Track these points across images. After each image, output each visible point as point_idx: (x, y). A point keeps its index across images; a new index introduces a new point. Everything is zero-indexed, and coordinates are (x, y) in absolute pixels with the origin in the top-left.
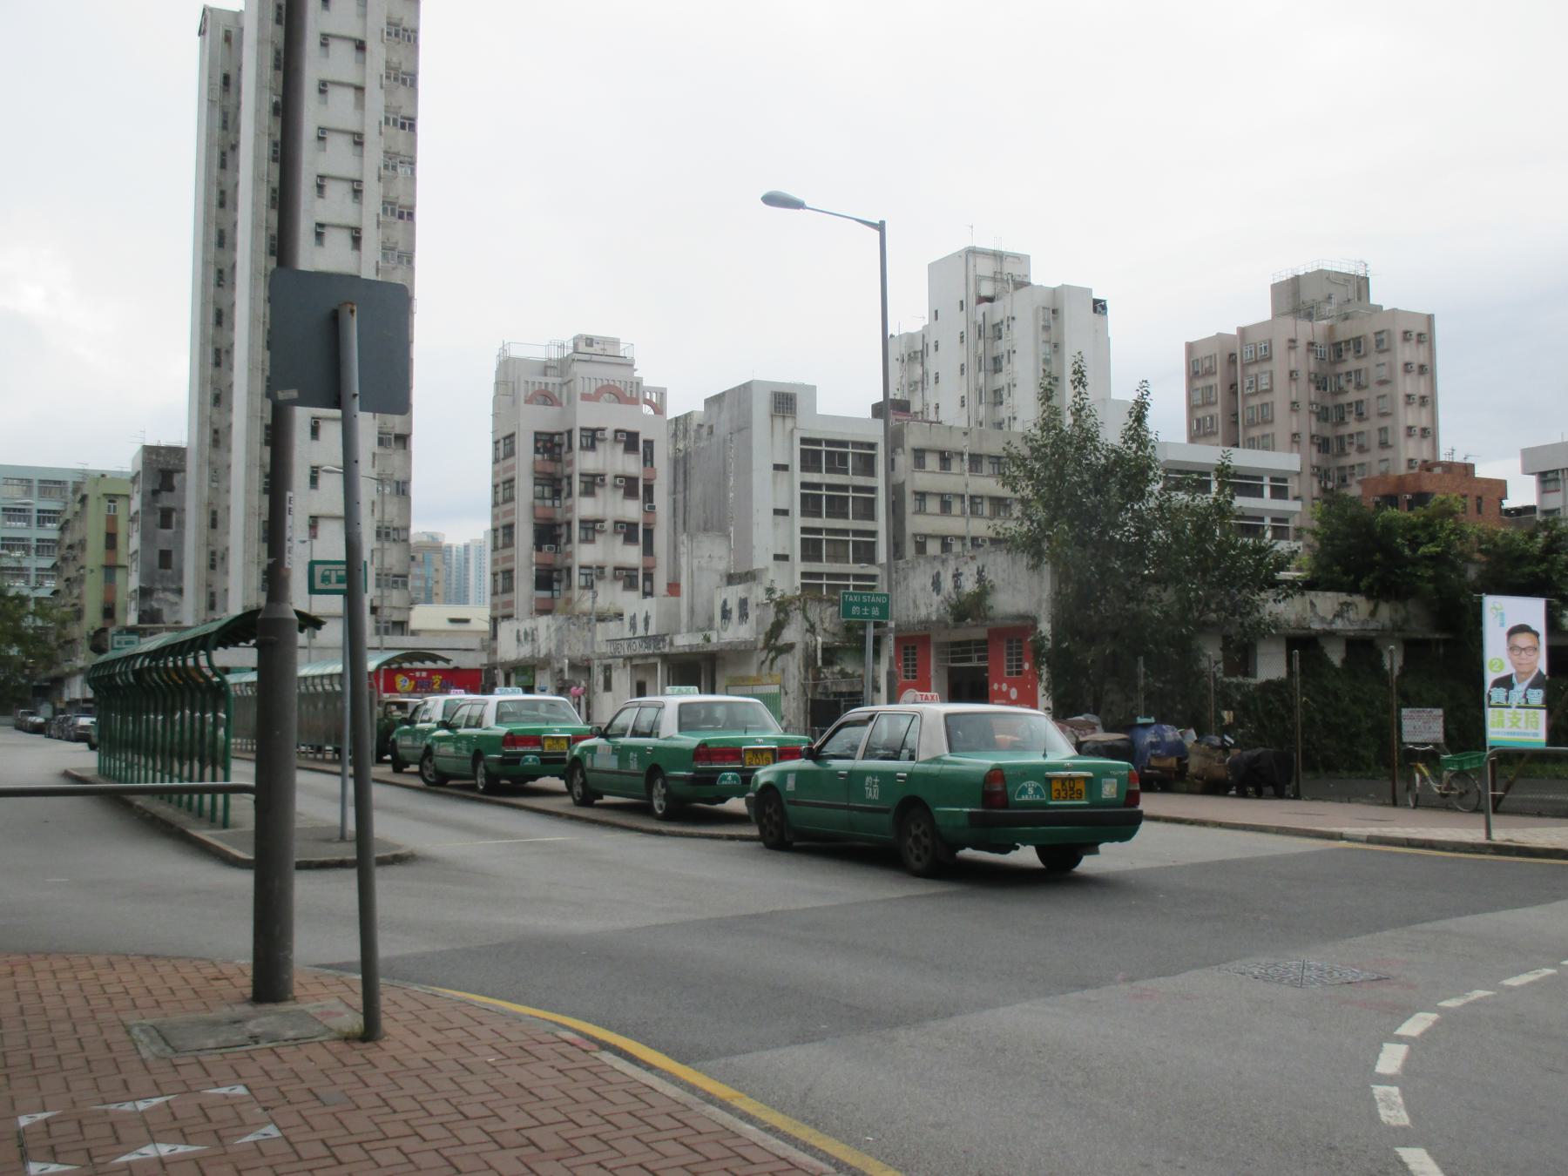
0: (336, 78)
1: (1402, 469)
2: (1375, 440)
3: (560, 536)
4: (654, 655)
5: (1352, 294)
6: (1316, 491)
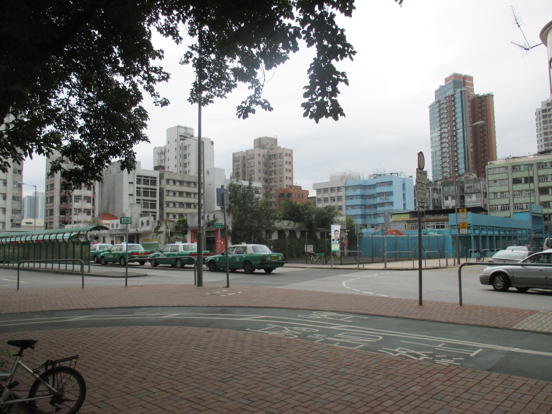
1: (285, 187)
2: (278, 180)
3: (68, 200)
4: (123, 234)
6: (264, 192)
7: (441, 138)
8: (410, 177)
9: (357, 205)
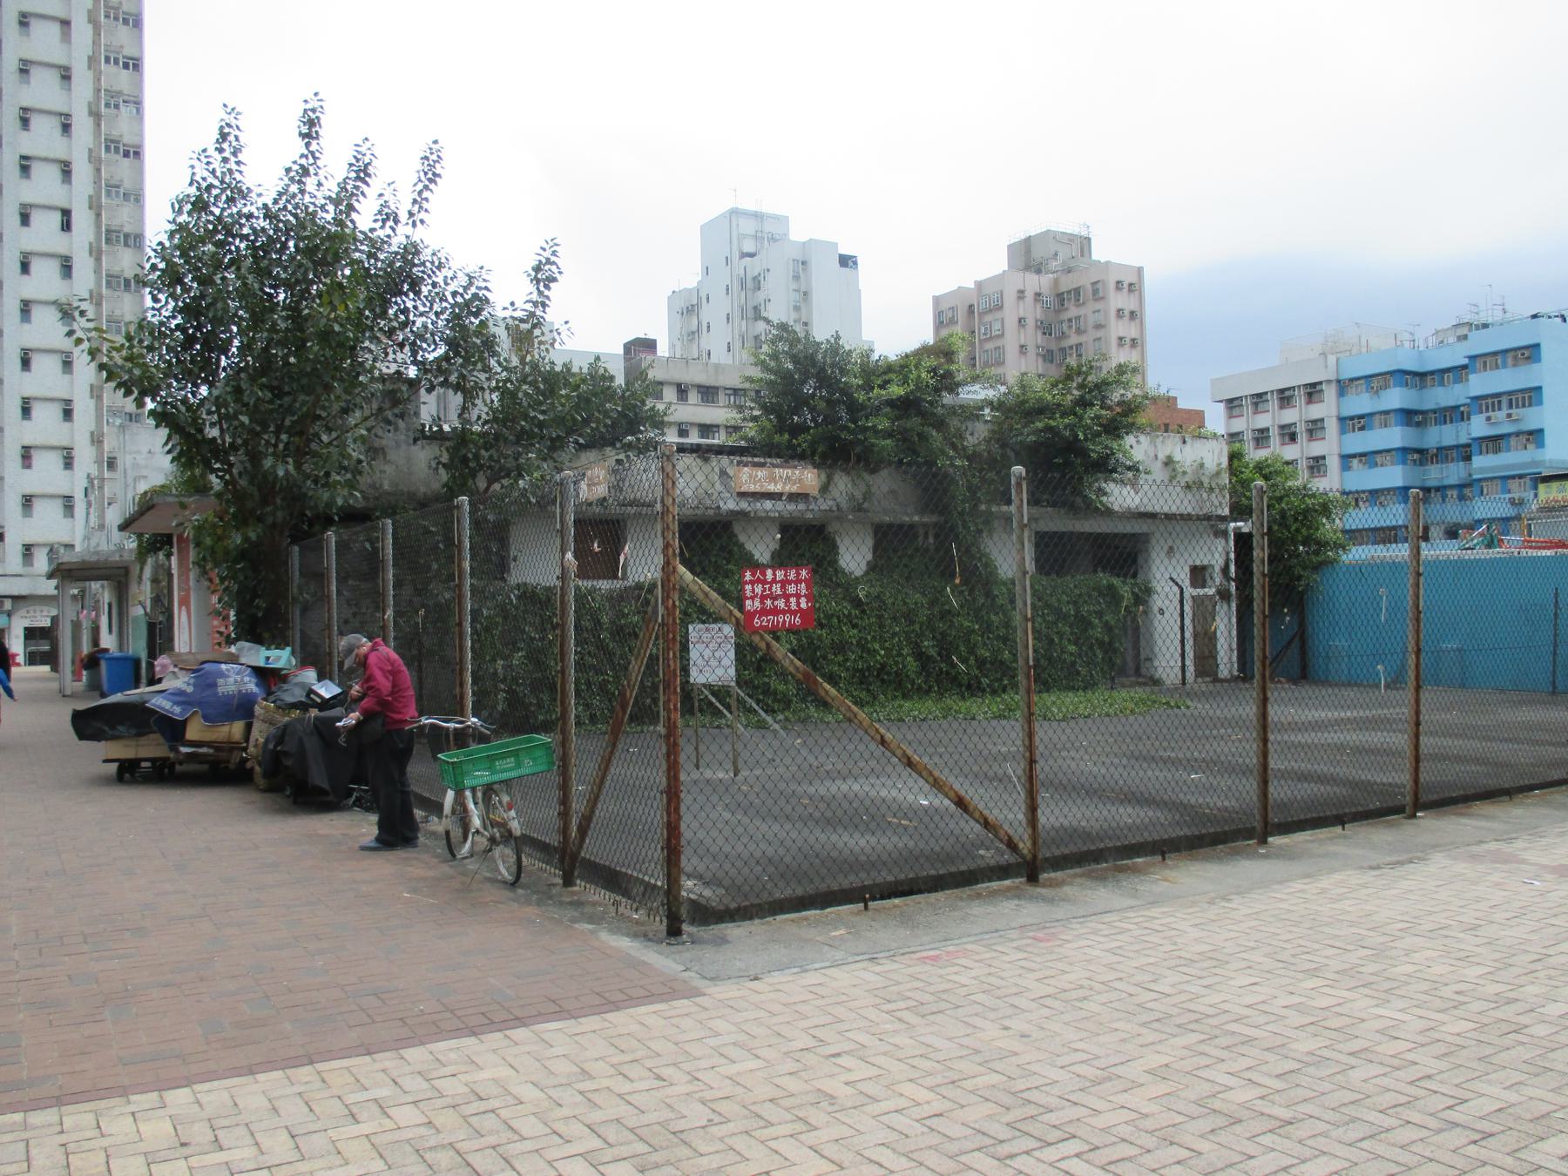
0: (40, 10)
5: (1075, 251)
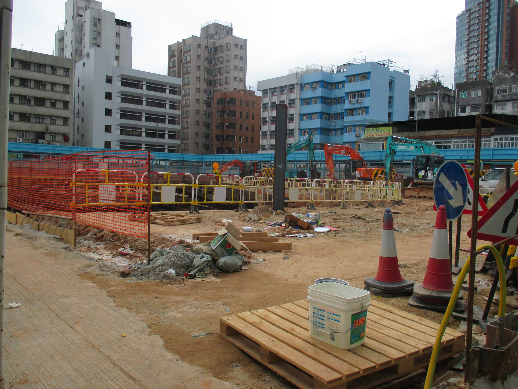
7: (469, 56)
8: (405, 71)
9: (316, 113)
